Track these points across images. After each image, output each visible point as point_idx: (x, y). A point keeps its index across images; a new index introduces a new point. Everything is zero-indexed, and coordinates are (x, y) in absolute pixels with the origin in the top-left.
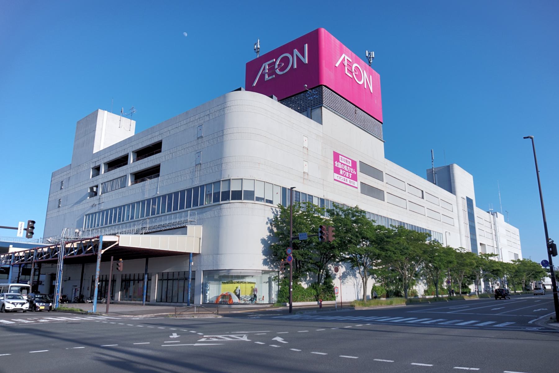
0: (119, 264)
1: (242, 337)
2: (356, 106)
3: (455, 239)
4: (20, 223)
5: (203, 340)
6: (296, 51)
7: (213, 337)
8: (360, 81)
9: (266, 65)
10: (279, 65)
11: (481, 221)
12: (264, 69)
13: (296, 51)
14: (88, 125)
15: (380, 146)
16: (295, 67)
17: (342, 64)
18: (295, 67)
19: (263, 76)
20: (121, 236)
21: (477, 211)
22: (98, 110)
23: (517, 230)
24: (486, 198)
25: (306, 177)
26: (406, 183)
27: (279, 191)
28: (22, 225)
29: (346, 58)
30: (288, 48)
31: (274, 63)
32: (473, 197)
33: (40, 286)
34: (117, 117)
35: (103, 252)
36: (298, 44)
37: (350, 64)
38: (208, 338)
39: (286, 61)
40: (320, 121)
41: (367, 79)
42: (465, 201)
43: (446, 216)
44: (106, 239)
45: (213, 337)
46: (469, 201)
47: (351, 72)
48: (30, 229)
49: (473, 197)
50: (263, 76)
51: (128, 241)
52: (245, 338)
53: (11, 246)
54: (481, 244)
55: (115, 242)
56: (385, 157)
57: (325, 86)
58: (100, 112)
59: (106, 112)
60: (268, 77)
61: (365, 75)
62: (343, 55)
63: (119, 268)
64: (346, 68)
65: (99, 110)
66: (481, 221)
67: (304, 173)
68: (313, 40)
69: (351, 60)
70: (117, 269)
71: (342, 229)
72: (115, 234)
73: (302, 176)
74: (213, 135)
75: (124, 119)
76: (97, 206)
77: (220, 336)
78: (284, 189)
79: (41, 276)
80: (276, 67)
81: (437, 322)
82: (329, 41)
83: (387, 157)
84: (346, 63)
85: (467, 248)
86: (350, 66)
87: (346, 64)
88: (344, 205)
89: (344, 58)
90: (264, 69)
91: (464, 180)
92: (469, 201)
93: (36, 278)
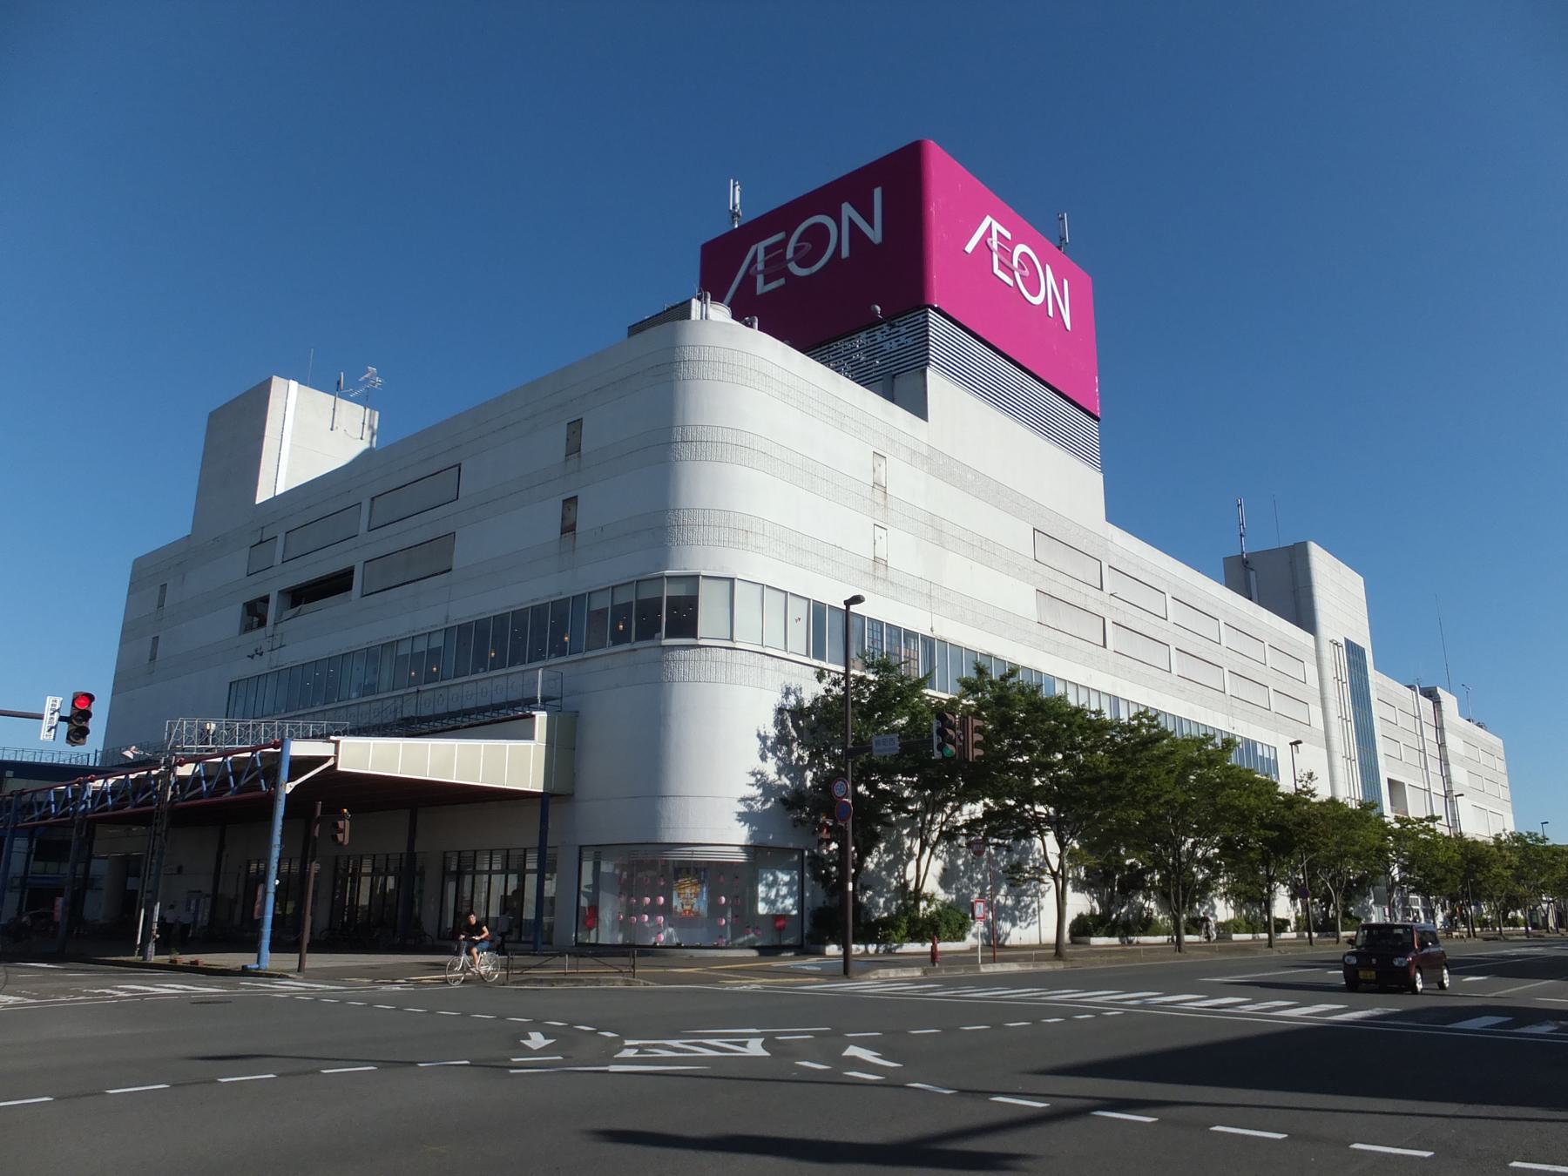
0: (341, 824)
1: (744, 1045)
2: (1030, 362)
3: (1310, 762)
4: (49, 700)
5: (631, 1053)
6: (847, 210)
7: (654, 1046)
8: (1035, 293)
9: (760, 247)
10: (796, 250)
11: (1389, 714)
12: (754, 260)
13: (847, 210)
14: (239, 430)
15: (1094, 481)
16: (845, 253)
17: (984, 242)
18: (845, 253)
19: (749, 280)
20: (345, 741)
21: (1375, 678)
22: (269, 381)
23: (1497, 742)
24: (1413, 641)
25: (881, 572)
26: (1168, 597)
27: (799, 611)
28: (54, 705)
29: (996, 227)
30: (827, 198)
31: (783, 244)
32: (1364, 640)
33: (90, 895)
34: (325, 399)
35: (289, 788)
36: (854, 188)
37: (1006, 248)
38: (640, 1049)
39: (818, 236)
40: (917, 406)
41: (1050, 292)
42: (1343, 653)
43: (1273, 693)
44: (300, 748)
45: (654, 1046)
46: (1354, 651)
47: (1010, 271)
48: (77, 723)
49: (1364, 640)
50: (749, 280)
51: (365, 755)
52: (755, 1048)
53: (9, 773)
54: (1390, 781)
55: (327, 758)
56: (1108, 519)
57: (937, 310)
58: (277, 383)
59: (294, 384)
60: (766, 282)
61: (1048, 279)
62: (988, 220)
63: (340, 836)
64: (995, 257)
65: (275, 379)
66: (1389, 714)
67: (875, 560)
68: (899, 178)
69: (1008, 235)
70: (335, 838)
71: (833, 759)
72: (324, 737)
73: (870, 570)
74: (636, 436)
75: (344, 405)
76: (266, 655)
77: (675, 1043)
78: (818, 611)
79: (94, 863)
80: (790, 254)
81: (648, 1046)
82: (944, 177)
83: (1113, 516)
84: (994, 243)
85: (1349, 792)
86: (1006, 253)
87: (995, 246)
88: (990, 656)
89: (989, 232)
90: (754, 260)
91: (1338, 589)
92: (1354, 651)
93: (80, 868)
